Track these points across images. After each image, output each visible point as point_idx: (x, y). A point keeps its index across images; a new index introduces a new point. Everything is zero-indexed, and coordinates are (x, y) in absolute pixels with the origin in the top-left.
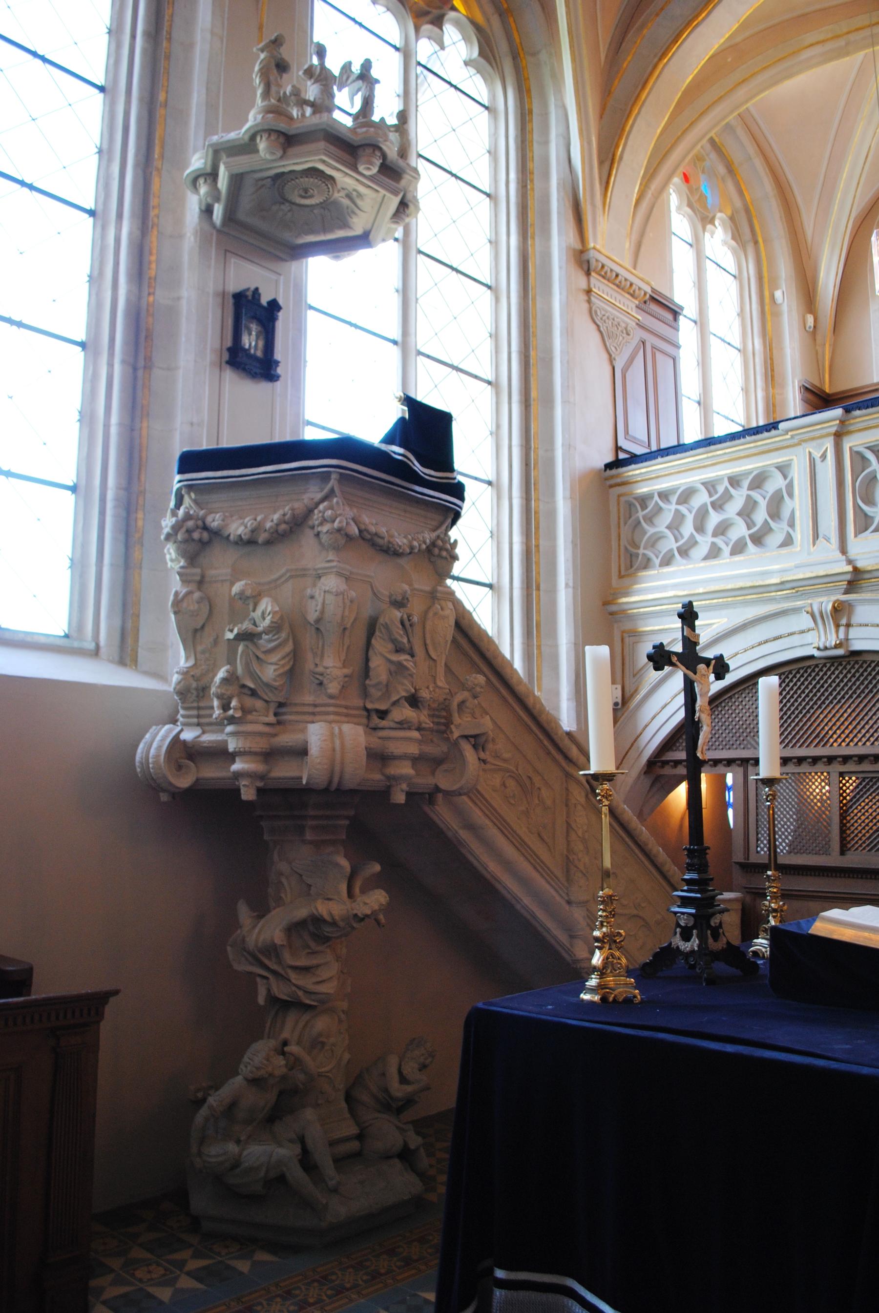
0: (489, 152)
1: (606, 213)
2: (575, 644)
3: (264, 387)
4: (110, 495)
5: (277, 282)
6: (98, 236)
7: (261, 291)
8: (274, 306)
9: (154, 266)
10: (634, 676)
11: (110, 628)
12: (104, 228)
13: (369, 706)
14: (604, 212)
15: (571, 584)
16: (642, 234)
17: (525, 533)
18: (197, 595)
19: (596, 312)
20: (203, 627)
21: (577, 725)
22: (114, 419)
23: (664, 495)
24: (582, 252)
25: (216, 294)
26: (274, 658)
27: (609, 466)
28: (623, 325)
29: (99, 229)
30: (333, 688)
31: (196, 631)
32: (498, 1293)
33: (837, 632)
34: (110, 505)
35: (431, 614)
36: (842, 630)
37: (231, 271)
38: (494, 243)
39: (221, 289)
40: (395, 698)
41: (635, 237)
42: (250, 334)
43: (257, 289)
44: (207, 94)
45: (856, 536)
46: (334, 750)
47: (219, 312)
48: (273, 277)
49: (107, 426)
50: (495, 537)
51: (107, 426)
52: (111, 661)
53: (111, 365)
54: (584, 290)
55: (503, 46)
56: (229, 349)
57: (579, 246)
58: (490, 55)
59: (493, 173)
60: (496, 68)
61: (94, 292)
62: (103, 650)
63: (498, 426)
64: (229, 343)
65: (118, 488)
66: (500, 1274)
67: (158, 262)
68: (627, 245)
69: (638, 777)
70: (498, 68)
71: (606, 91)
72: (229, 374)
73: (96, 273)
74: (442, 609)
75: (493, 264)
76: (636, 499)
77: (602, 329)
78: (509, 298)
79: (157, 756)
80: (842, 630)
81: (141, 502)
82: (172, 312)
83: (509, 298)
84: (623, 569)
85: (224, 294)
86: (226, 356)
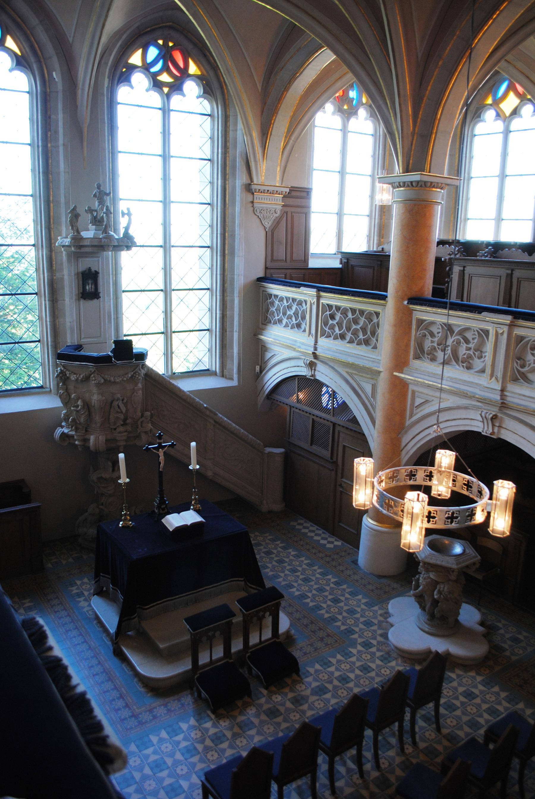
0: (210, 138)
1: (265, 160)
2: (238, 354)
3: (95, 301)
4: (49, 344)
5: (98, 261)
6: (37, 254)
7: (91, 268)
8: (97, 273)
9: (54, 265)
10: (264, 363)
11: (53, 384)
12: (38, 251)
13: (111, 427)
14: (264, 160)
15: (238, 331)
16: (287, 162)
17: (222, 309)
18: (65, 394)
19: (256, 210)
20: (68, 402)
21: (238, 383)
22: (48, 320)
23: (276, 296)
24: (250, 184)
25: (75, 275)
26: (83, 416)
27: (260, 280)
28: (273, 210)
29: (37, 251)
30: (98, 425)
31: (66, 403)
32: (101, 577)
33: (311, 371)
34: (50, 347)
35: (133, 395)
36: (313, 371)
37: (80, 264)
38: (212, 183)
39: (76, 272)
40: (117, 425)
41: (283, 164)
42: (89, 285)
43: (90, 268)
44: (65, 199)
45: (320, 337)
46: (96, 444)
47: (77, 280)
48: (96, 259)
49: (46, 321)
50: (210, 311)
51: (46, 321)
52: (55, 394)
53: (45, 300)
54: (250, 202)
55: (215, 84)
56: (81, 293)
57: (249, 182)
58: (210, 91)
59: (212, 149)
60: (213, 96)
61: (38, 275)
62: (52, 391)
63: (212, 265)
64: (81, 291)
65: (52, 342)
66: (101, 574)
67: (56, 264)
68: (278, 169)
69: (264, 400)
70: (214, 95)
71: (264, 103)
72: (82, 301)
73: (37, 268)
74: (137, 393)
75: (211, 193)
76: (268, 294)
77: (260, 217)
78: (217, 209)
79: (57, 438)
80: (313, 371)
81: (58, 346)
82: (62, 279)
83: (217, 209)
84: (263, 320)
85: (78, 273)
86: (81, 295)
